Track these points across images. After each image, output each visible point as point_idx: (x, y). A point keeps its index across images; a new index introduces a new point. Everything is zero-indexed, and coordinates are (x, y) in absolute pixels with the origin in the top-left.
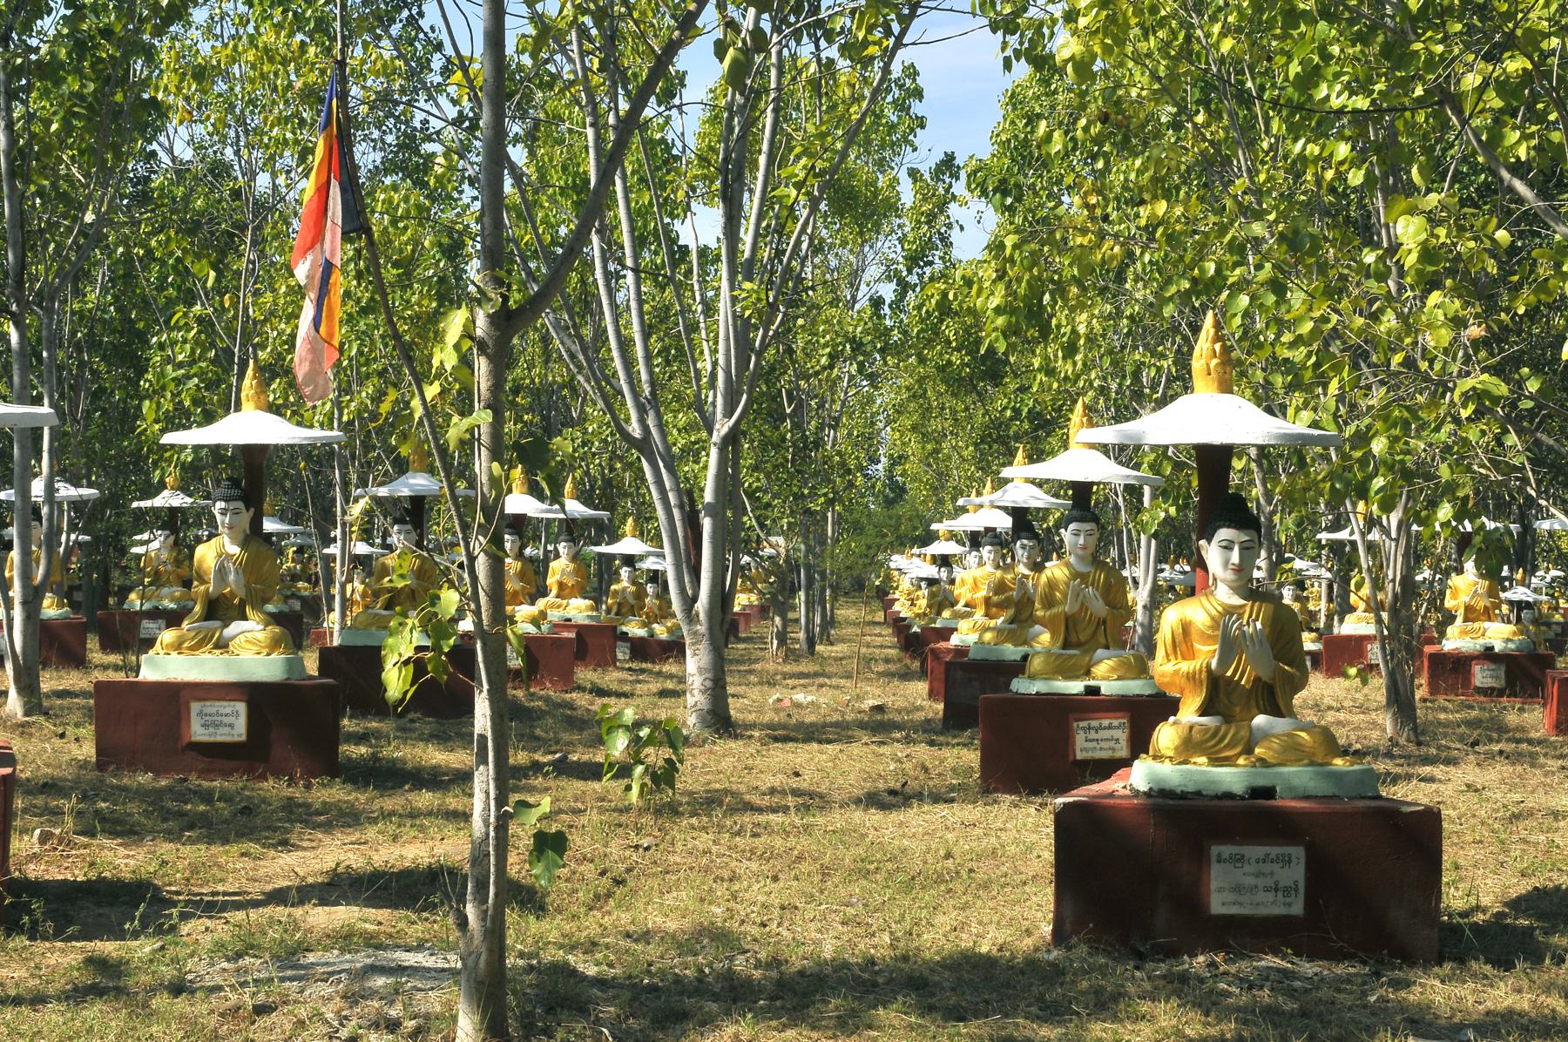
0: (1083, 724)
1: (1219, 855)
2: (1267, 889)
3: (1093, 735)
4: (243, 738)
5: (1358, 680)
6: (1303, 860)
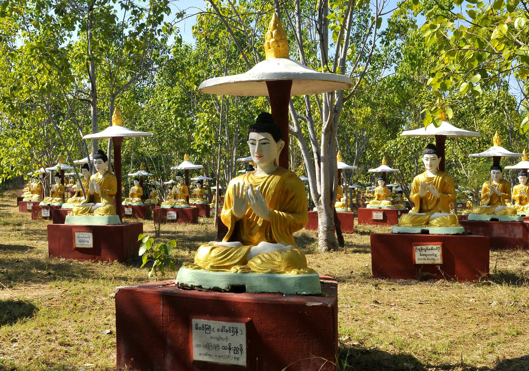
0: (418, 247)
1: (197, 325)
2: (224, 348)
3: (423, 252)
4: (92, 246)
5: (30, 214)
6: (244, 332)
